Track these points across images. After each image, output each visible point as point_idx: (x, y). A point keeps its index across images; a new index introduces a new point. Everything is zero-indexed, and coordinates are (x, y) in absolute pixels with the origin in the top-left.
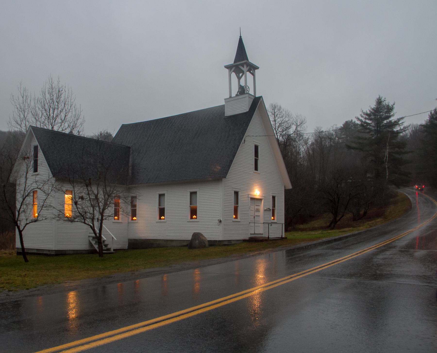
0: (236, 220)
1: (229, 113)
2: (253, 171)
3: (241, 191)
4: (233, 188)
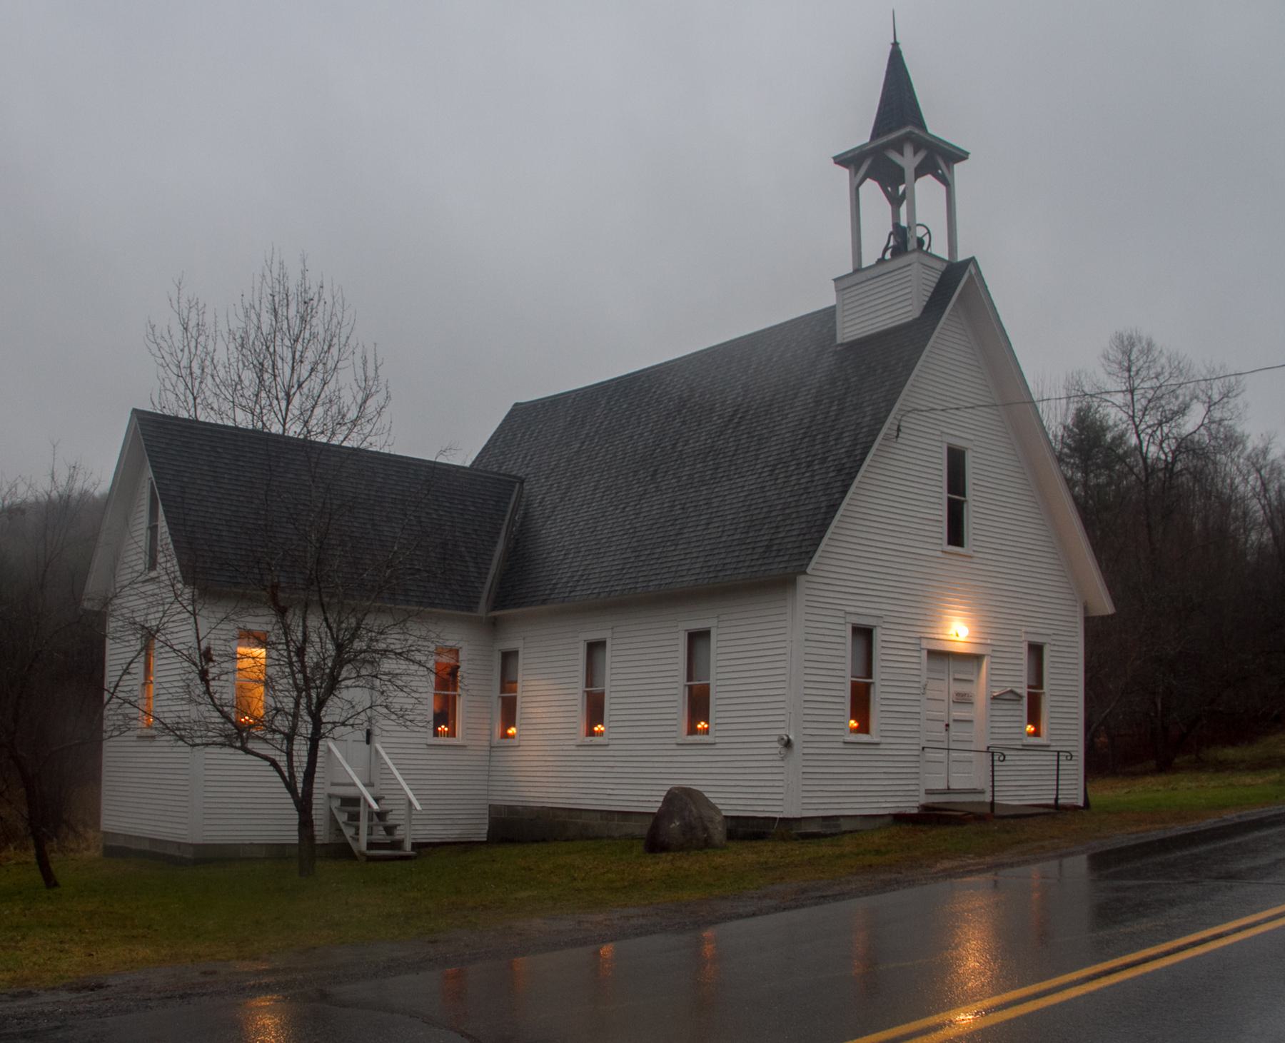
0: (863, 738)
1: (849, 331)
2: (940, 548)
4: (846, 613)
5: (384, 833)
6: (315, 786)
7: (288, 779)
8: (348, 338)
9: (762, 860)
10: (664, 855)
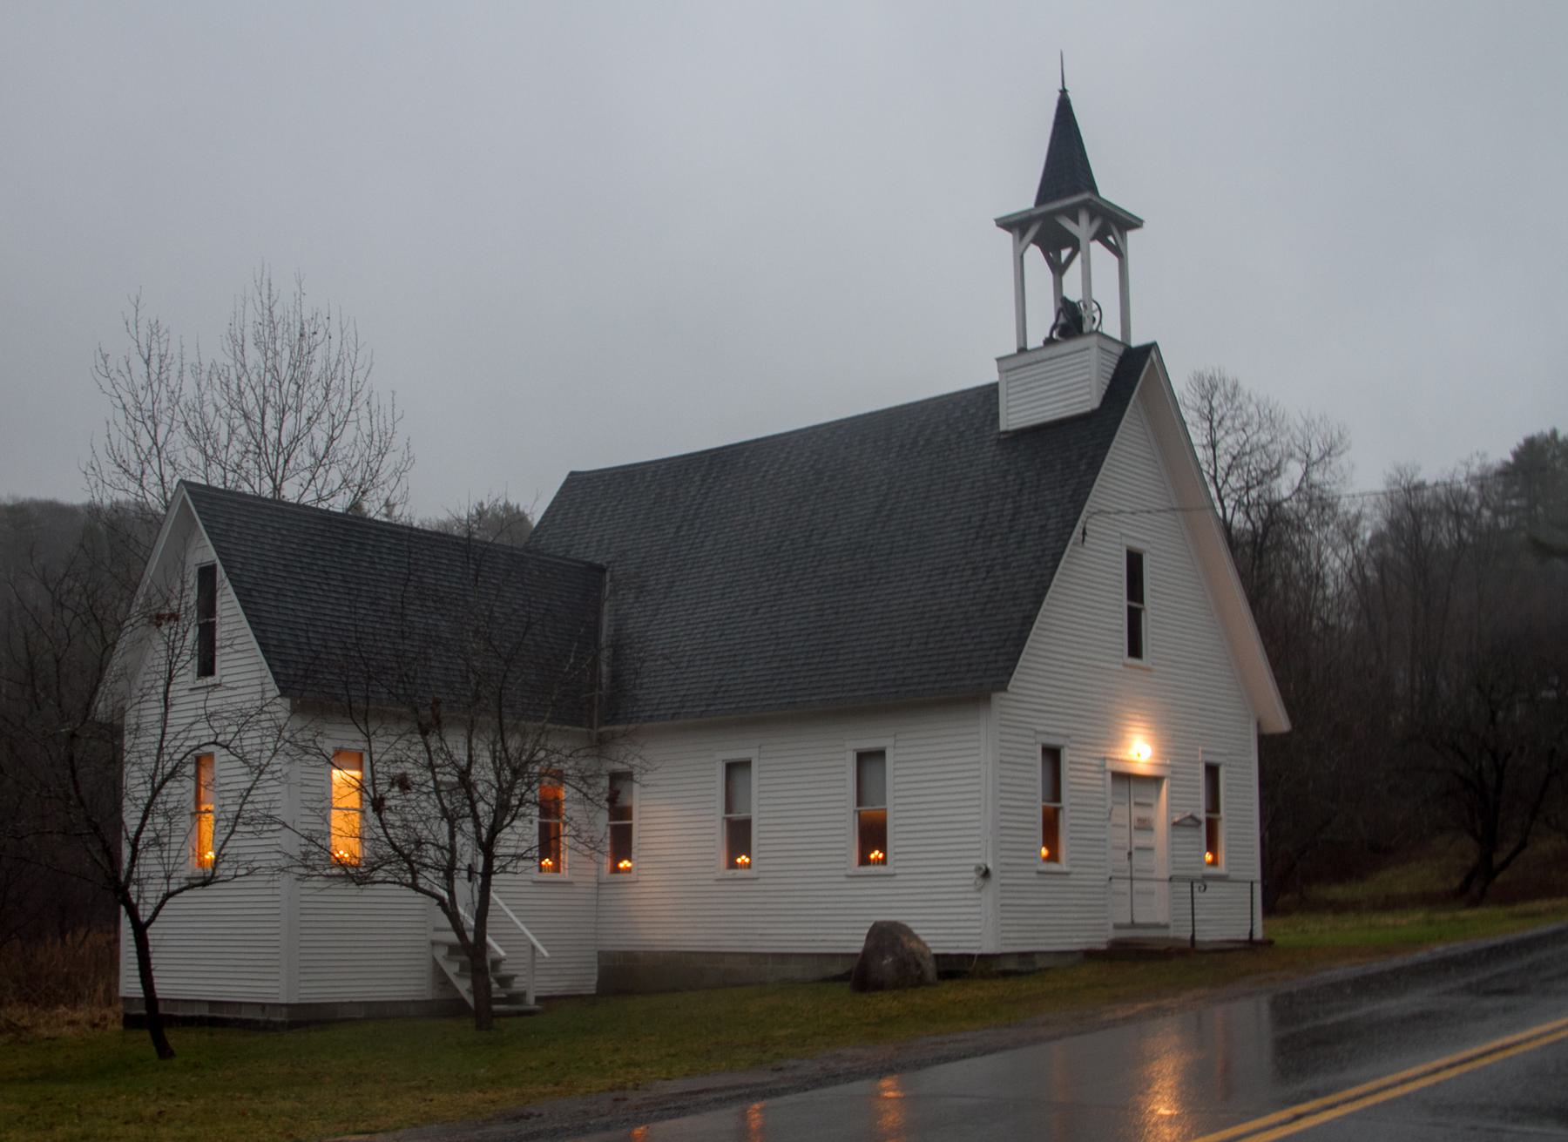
0: (1053, 867)
1: (1015, 415)
2: (1121, 661)
10: (879, 993)
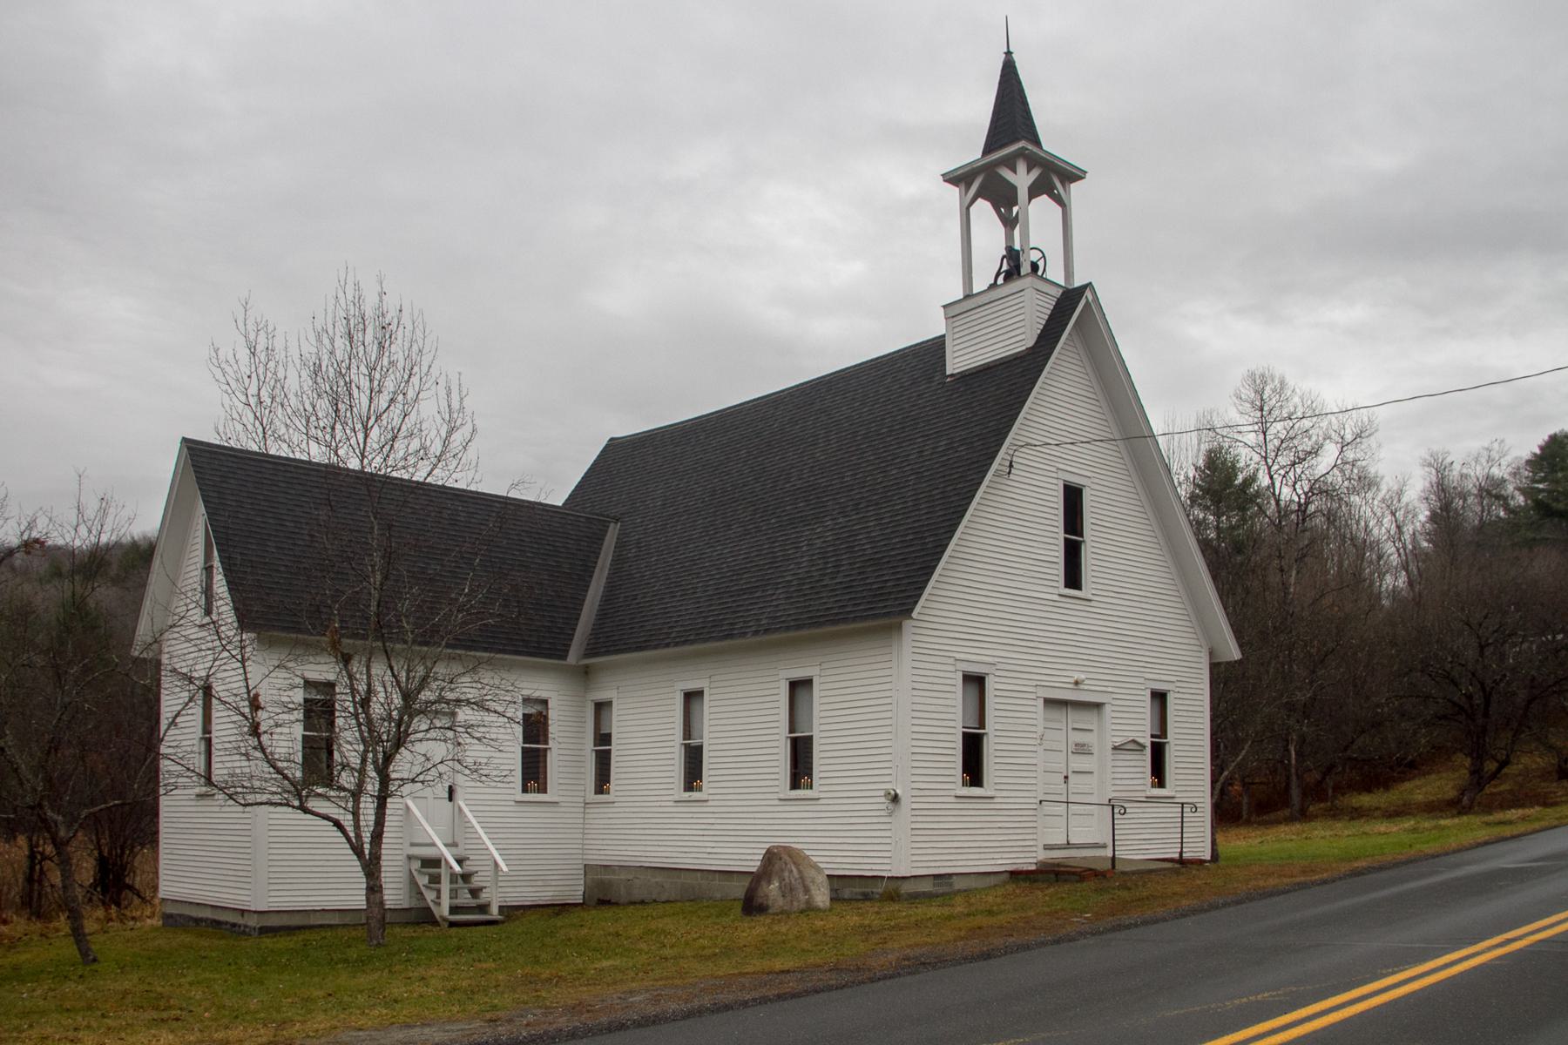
1: (957, 362)
2: (1056, 591)
3: (998, 673)
4: (956, 660)
5: (469, 896)
6: (383, 846)
7: (354, 841)
8: (430, 367)
9: (867, 922)
